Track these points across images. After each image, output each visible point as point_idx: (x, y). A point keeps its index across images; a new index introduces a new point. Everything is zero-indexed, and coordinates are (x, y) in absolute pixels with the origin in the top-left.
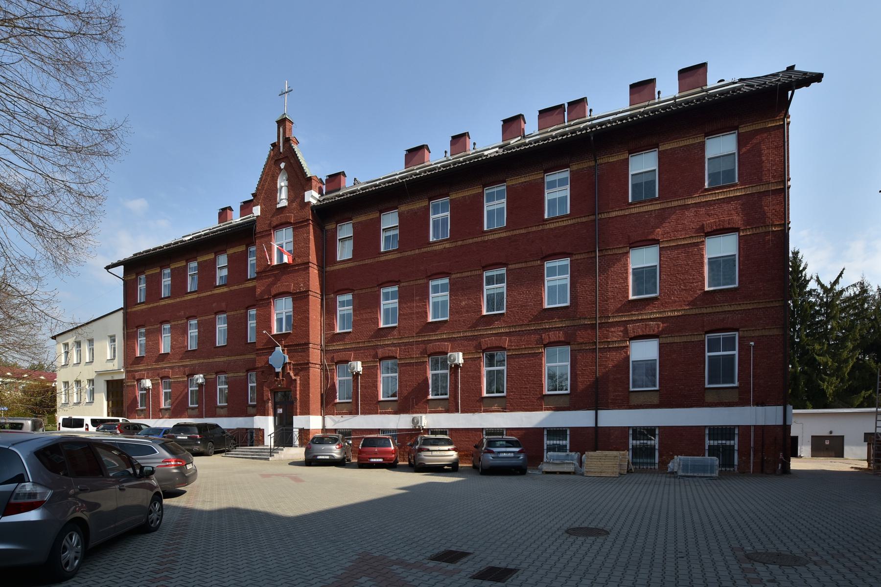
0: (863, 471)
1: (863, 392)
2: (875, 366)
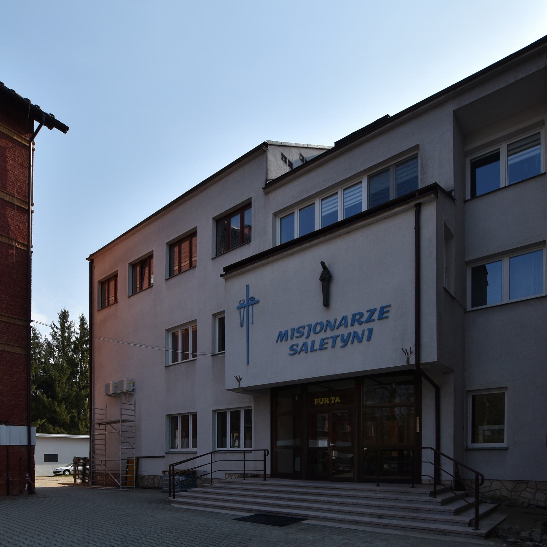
0: (71, 486)
1: (39, 421)
2: (47, 400)
